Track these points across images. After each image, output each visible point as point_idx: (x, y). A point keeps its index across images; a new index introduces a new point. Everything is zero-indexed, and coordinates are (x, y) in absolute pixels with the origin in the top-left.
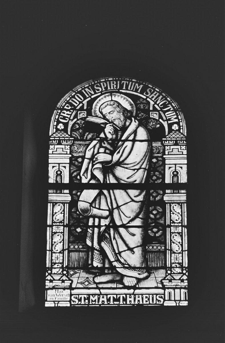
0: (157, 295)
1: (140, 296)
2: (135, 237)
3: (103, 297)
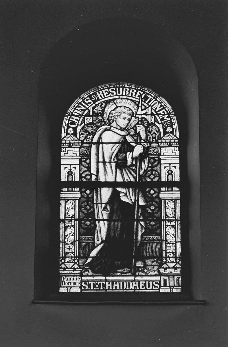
0: (153, 281)
1: (118, 283)
2: (64, 168)
3: (116, 284)
